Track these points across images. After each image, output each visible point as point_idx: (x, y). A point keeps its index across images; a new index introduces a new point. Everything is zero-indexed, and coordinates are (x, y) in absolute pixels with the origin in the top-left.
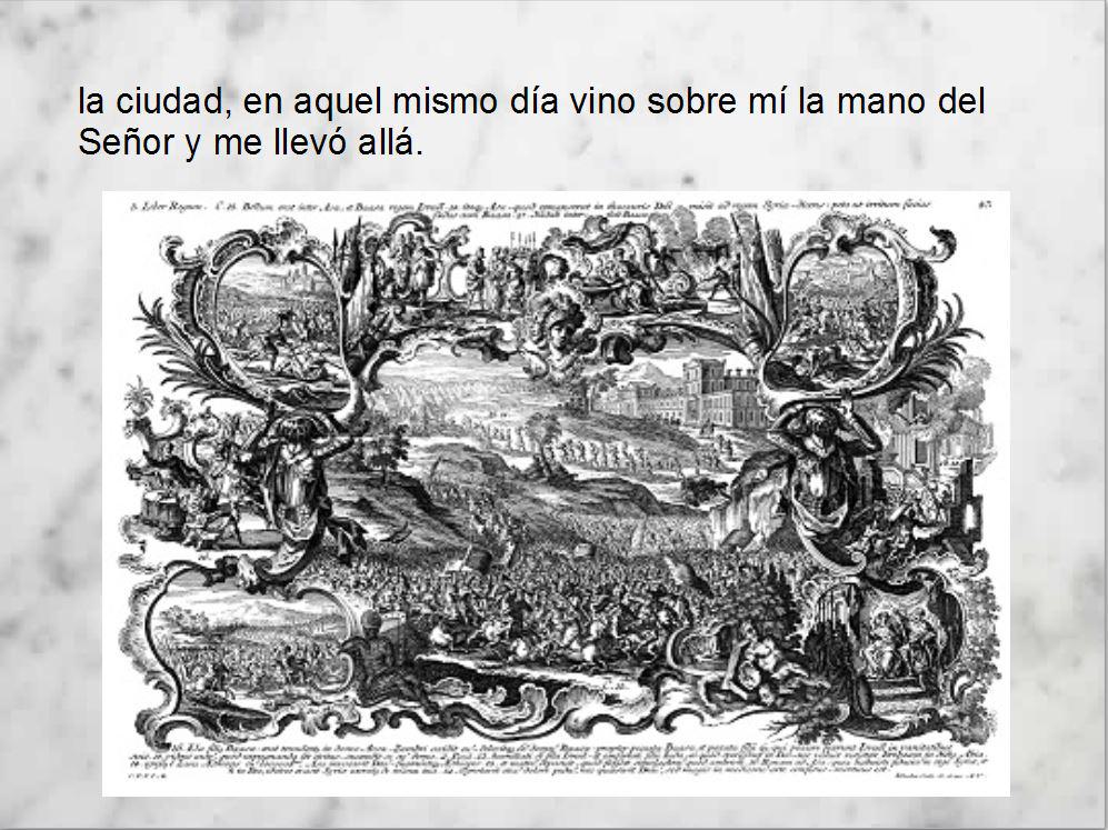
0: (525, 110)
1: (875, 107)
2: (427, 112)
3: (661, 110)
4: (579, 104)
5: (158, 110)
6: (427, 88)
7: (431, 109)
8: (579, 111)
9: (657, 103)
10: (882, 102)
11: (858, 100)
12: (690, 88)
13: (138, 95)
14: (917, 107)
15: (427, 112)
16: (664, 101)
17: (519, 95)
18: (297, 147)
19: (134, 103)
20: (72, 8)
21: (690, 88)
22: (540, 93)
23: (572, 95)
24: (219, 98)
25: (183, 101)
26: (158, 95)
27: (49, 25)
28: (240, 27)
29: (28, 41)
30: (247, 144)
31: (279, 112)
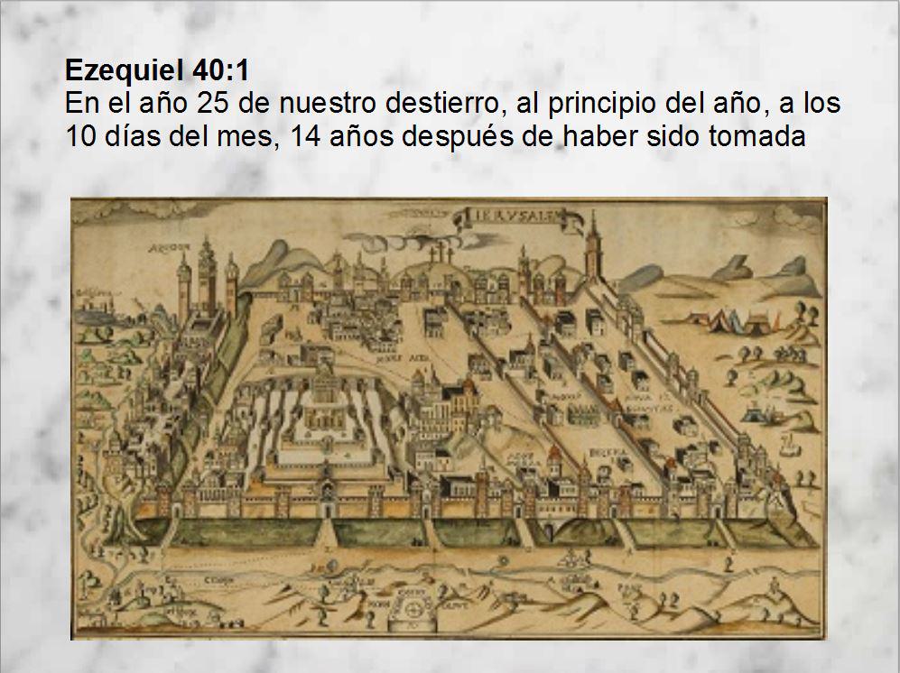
0: (117, 143)
1: (587, 141)
3: (340, 110)
6: (638, 92)
10: (725, 103)
11: (750, 135)
13: (614, 98)
14: (649, 108)
16: (826, 105)
17: (676, 131)
18: (687, 107)
19: (611, 104)
22: (130, 130)
24: (551, 109)
25: (791, 137)
26: (308, 98)
27: (40, 21)
28: (195, 24)
29: (24, 34)
30: (244, 138)
31: (97, 112)
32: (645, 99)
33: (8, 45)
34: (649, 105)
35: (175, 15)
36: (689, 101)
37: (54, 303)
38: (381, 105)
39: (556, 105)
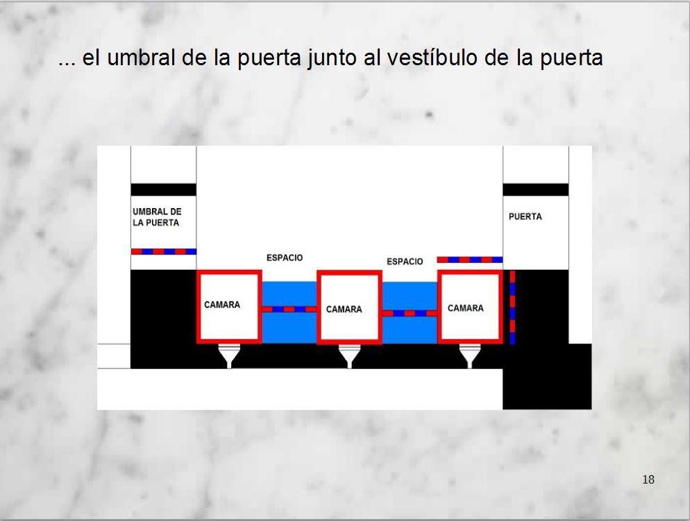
4: (393, 60)
6: (311, 50)
8: (393, 64)
12: (141, 49)
17: (490, 54)
18: (569, 61)
20: (44, 6)
21: (141, 49)
23: (389, 54)
24: (543, 62)
27: (30, 17)
29: (17, 28)
34: (472, 59)
35: (134, 12)
36: (503, 56)
38: (481, 59)
39: (546, 59)
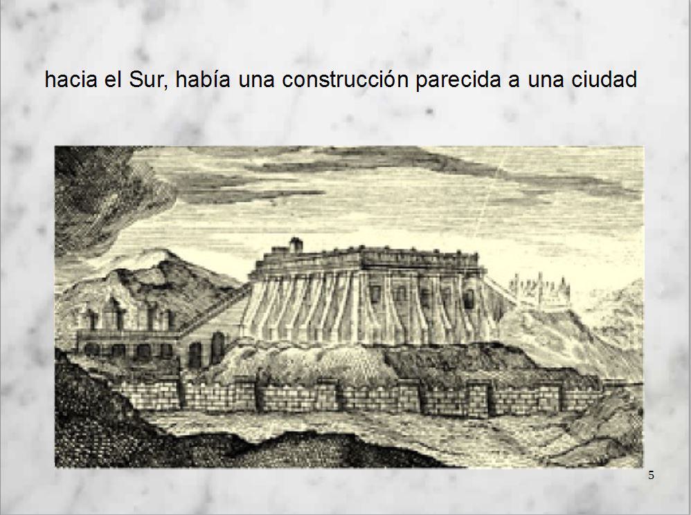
2: (316, 86)
5: (597, 85)
6: (475, 72)
7: (318, 84)
9: (270, 81)
10: (437, 80)
12: (202, 72)
13: (585, 76)
15: (316, 86)
19: (379, 81)
21: (202, 72)
22: (219, 75)
24: (418, 84)
27: (31, 15)
29: (18, 25)
31: (407, 86)
32: (628, 77)
33: (6, 33)
37: (42, 231)
39: (422, 81)
